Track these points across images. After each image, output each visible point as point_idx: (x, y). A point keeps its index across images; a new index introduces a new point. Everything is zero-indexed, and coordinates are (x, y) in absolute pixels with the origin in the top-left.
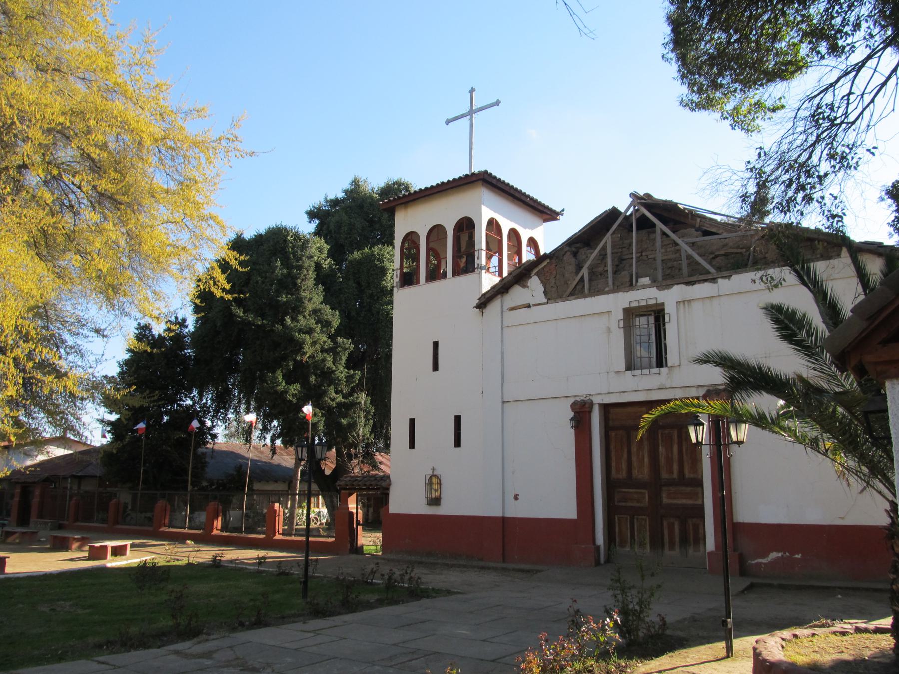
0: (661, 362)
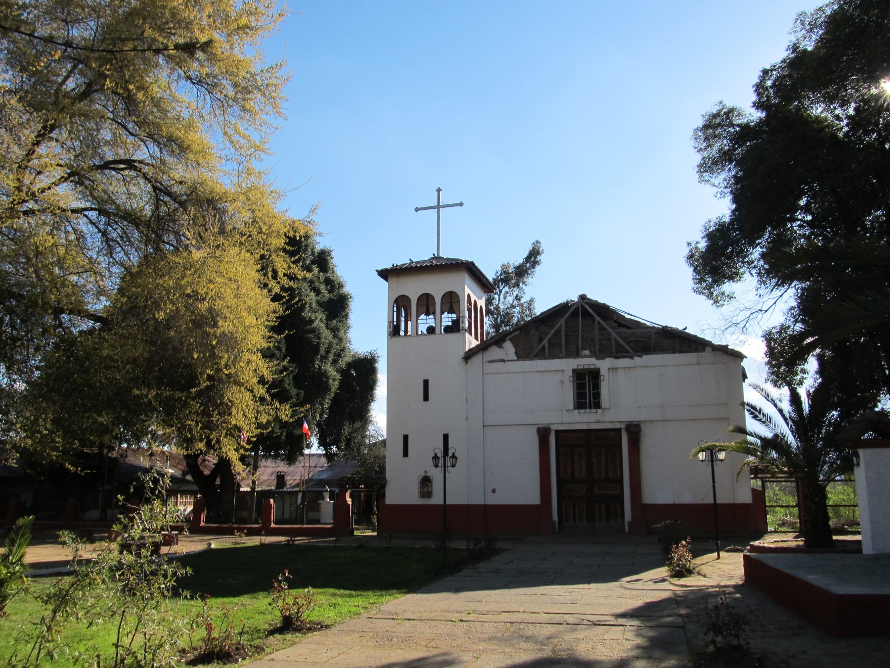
0: (597, 405)
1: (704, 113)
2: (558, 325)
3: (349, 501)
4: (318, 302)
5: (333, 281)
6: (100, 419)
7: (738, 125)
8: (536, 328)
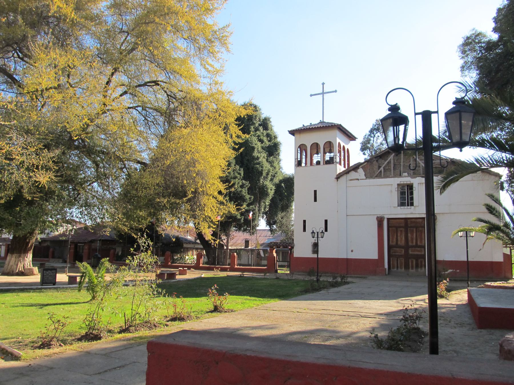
0: (412, 204)
1: (463, 36)
2: (389, 159)
3: (275, 255)
4: (262, 148)
5: (271, 135)
6: (141, 213)
7: (484, 42)
8: (377, 161)
